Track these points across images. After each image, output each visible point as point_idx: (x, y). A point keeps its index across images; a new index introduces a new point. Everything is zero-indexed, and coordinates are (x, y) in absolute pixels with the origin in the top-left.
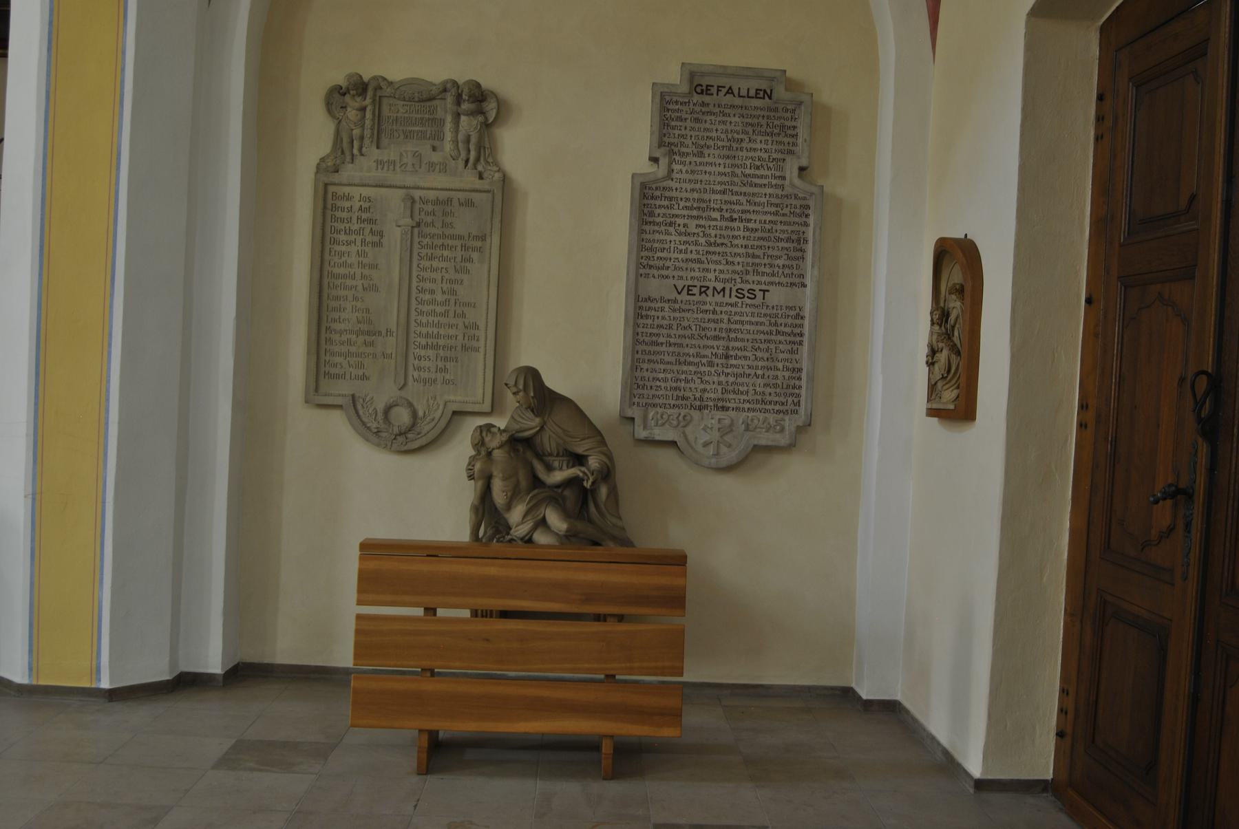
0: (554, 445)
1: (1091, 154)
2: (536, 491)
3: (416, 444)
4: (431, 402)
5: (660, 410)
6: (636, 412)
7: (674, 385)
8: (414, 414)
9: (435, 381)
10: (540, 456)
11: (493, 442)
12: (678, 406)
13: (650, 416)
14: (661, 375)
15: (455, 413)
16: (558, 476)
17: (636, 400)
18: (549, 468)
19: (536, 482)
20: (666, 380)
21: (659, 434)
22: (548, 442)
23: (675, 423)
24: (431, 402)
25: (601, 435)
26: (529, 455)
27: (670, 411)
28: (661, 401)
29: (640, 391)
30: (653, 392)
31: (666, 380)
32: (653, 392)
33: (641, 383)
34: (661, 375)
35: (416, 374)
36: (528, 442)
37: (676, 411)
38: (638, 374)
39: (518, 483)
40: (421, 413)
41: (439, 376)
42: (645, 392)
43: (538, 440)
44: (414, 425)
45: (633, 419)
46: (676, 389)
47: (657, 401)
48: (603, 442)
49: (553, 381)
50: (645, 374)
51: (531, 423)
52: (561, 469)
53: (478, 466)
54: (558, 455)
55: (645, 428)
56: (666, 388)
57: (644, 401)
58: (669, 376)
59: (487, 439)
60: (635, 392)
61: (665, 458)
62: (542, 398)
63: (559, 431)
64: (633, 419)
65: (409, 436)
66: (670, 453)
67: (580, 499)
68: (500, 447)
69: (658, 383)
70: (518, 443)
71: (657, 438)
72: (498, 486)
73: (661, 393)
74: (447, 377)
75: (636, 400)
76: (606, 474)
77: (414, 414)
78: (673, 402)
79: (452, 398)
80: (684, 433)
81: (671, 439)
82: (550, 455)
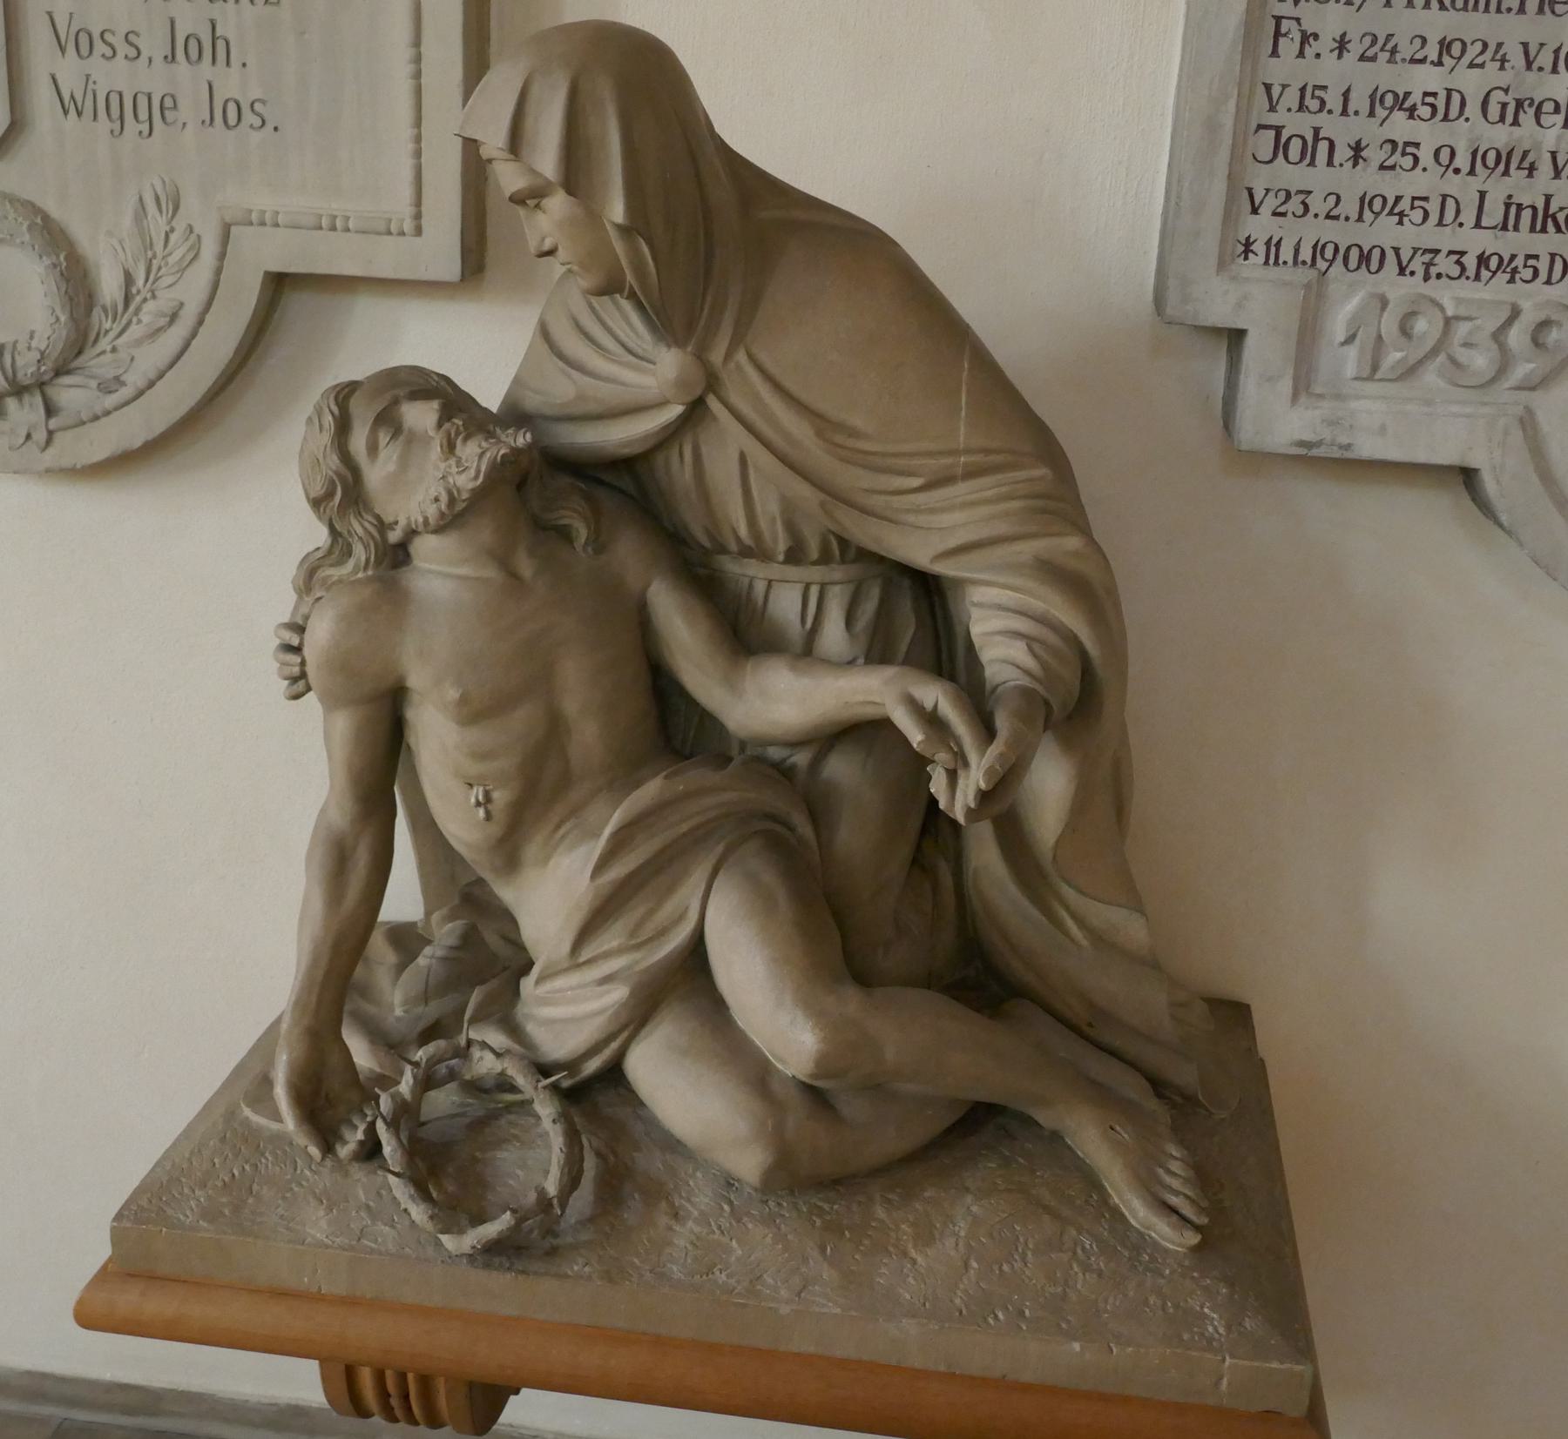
0: (768, 507)
1: (1176, 70)
2: (650, 790)
3: (132, 428)
4: (157, 223)
5: (1399, 289)
6: (1257, 301)
7: (1499, 136)
8: (75, 281)
9: (167, 106)
10: (700, 570)
11: (420, 480)
12: (1507, 267)
13: (1338, 323)
14: (1427, 79)
15: (279, 284)
16: (775, 702)
17: (1260, 227)
18: (744, 634)
19: (671, 725)
20: (1446, 106)
21: (1378, 424)
22: (733, 479)
23: (1481, 361)
24: (157, 223)
25: (1045, 446)
26: (630, 554)
27: (1450, 295)
28: (1408, 236)
29: (1290, 175)
30: (1367, 179)
31: (1446, 106)
32: (1367, 179)
33: (1298, 125)
34: (1427, 79)
35: (70, 71)
36: (626, 487)
37: (1497, 289)
38: (1285, 69)
39: (555, 729)
40: (109, 286)
41: (188, 80)
42: (1318, 178)
43: (679, 470)
44: (79, 342)
45: (1235, 338)
46: (1504, 160)
47: (1383, 232)
48: (1059, 500)
49: (763, 114)
50: (1331, 71)
51: (630, 380)
52: (806, 652)
53: (321, 632)
54: (795, 556)
55: (1302, 386)
56: (1445, 157)
57: (1313, 231)
58: (1471, 83)
59: (376, 474)
60: (1260, 179)
61: (1402, 551)
62: (705, 226)
63: (798, 428)
64: (1235, 338)
65: (70, 395)
66: (1430, 517)
67: (902, 901)
68: (453, 518)
69: (1401, 128)
70: (563, 492)
71: (1369, 447)
72: (445, 755)
73: (1409, 184)
74: (230, 84)
75: (1260, 227)
76: (1077, 701)
77: (75, 281)
78: (1476, 242)
79: (262, 201)
80: (1528, 422)
81: (1446, 455)
82: (756, 551)
